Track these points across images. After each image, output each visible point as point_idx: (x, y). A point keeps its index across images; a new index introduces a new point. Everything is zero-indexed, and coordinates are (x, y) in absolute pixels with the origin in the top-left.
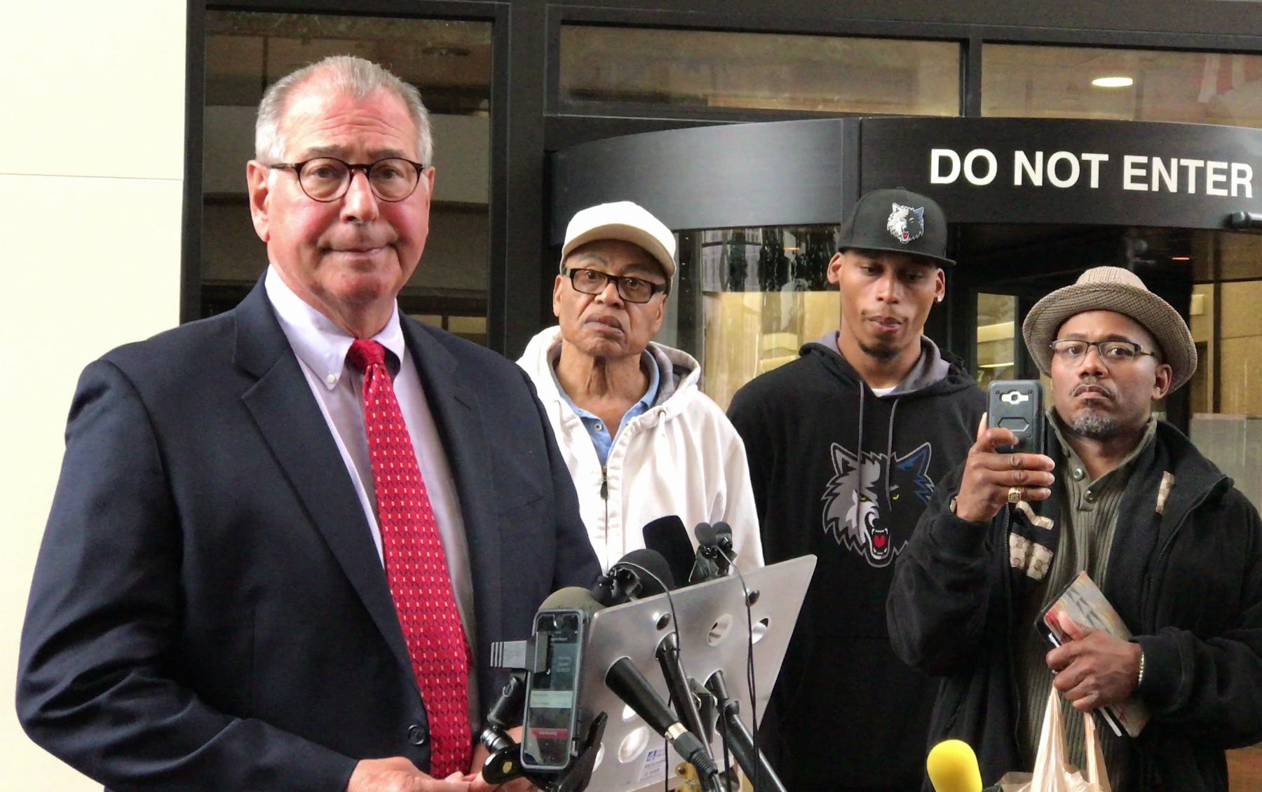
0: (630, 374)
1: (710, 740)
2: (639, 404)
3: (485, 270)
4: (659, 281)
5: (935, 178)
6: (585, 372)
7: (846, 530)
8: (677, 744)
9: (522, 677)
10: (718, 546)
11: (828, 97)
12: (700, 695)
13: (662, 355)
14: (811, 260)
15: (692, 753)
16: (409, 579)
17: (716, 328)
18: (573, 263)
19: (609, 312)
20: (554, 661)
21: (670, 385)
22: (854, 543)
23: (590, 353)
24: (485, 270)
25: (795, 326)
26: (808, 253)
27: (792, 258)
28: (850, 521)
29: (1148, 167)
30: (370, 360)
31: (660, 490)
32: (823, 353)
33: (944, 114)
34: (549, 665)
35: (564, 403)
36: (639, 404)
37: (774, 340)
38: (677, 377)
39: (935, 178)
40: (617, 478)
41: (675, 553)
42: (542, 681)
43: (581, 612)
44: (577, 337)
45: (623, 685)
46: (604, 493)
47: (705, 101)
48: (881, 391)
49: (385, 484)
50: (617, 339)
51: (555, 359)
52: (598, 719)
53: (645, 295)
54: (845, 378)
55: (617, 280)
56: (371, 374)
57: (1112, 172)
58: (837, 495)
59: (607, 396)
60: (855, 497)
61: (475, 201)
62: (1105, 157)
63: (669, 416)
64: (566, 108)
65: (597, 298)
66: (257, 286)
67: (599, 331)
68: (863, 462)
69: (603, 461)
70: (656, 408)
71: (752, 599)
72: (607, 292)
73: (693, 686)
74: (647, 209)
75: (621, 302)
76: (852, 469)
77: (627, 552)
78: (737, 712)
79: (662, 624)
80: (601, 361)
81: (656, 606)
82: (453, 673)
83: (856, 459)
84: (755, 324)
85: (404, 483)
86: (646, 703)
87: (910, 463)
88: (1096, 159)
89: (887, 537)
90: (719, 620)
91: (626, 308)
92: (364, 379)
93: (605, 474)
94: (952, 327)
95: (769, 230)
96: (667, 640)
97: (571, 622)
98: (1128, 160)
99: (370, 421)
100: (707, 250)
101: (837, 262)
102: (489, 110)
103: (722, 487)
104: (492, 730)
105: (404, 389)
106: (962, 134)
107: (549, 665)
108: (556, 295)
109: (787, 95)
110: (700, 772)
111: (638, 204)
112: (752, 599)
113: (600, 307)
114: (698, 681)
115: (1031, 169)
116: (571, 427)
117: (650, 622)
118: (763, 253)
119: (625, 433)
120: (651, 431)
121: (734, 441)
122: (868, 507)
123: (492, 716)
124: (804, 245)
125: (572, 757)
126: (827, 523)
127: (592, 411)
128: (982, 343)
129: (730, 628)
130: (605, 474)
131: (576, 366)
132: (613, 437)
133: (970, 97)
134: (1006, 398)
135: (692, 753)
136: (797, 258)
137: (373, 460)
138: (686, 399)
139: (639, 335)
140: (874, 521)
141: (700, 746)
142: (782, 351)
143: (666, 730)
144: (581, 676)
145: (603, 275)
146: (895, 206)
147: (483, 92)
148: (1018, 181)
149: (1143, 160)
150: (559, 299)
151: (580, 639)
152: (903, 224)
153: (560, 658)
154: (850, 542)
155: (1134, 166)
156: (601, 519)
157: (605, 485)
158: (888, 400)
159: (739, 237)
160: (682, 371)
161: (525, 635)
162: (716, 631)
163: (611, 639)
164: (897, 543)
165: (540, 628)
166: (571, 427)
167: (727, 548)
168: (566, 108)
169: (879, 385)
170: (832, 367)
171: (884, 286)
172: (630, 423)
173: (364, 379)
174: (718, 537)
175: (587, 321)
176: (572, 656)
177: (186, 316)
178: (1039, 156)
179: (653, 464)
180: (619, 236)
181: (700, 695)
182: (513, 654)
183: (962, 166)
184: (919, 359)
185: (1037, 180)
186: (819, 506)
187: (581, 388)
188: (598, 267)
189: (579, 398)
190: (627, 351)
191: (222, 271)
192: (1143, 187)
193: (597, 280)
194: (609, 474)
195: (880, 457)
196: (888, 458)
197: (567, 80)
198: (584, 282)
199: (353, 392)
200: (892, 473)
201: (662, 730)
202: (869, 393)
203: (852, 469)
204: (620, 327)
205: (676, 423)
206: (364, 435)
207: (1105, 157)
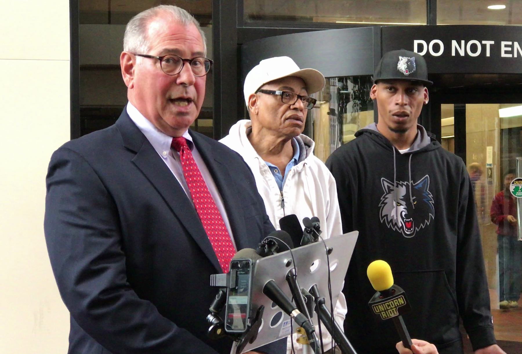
1: (311, 316)
2: (293, 160)
7: (392, 220)
8: (296, 319)
9: (225, 290)
10: (314, 227)
12: (306, 296)
14: (361, 93)
15: (303, 323)
17: (317, 123)
22: (396, 227)
26: (359, 90)
28: (393, 216)
29: (512, 46)
34: (237, 284)
36: (293, 160)
42: (234, 291)
43: (251, 260)
45: (270, 292)
48: (402, 151)
52: (260, 309)
57: (496, 49)
60: (394, 203)
62: (493, 42)
64: (246, 24)
68: (397, 187)
69: (281, 189)
71: (329, 252)
73: (303, 293)
76: (392, 190)
78: (324, 303)
79: (288, 264)
81: (286, 256)
87: (420, 186)
93: (282, 195)
94: (430, 119)
95: (341, 79)
96: (291, 272)
97: (246, 265)
98: (503, 43)
101: (375, 89)
103: (328, 198)
104: (212, 315)
105: (195, 155)
106: (428, 33)
107: (237, 284)
109: (348, 16)
110: (307, 331)
114: (305, 289)
115: (460, 48)
117: (283, 263)
119: (289, 175)
120: (299, 173)
122: (402, 208)
123: (212, 308)
125: (248, 326)
126: (382, 218)
133: (431, 15)
135: (303, 323)
136: (354, 92)
140: (405, 215)
141: (307, 319)
144: (251, 289)
147: (209, 17)
148: (453, 54)
149: (510, 43)
153: (242, 281)
155: (506, 46)
158: (407, 155)
168: (246, 24)
169: (401, 148)
170: (377, 140)
171: (399, 98)
174: (314, 224)
177: (74, 134)
178: (463, 42)
179: (303, 190)
181: (306, 296)
185: (462, 53)
186: (378, 209)
192: (510, 56)
194: (284, 195)
195: (405, 183)
196: (410, 185)
200: (416, 192)
201: (289, 313)
202: (397, 152)
203: (392, 190)
207: (493, 42)
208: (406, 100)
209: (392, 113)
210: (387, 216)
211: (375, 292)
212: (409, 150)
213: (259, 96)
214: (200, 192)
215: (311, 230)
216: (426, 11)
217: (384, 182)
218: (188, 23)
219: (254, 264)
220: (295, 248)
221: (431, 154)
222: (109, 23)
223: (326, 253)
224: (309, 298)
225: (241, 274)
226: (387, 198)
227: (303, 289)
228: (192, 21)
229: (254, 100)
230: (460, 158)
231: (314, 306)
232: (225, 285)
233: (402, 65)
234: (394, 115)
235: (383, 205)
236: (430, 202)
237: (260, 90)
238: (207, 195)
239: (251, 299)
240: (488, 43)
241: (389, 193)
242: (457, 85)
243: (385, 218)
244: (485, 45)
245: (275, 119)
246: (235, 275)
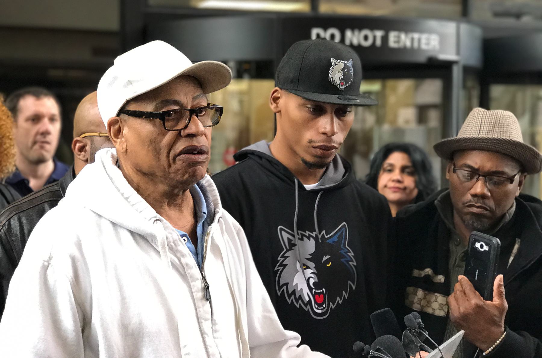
7: (294, 292)
22: (300, 302)
48: (309, 187)
57: (385, 39)
68: (302, 239)
74: (188, 57)
87: (336, 239)
88: (379, 34)
122: (309, 272)
126: (280, 288)
134: (478, 245)
146: (333, 61)
152: (341, 75)
154: (297, 301)
158: (314, 192)
164: (332, 299)
202: (301, 187)
210: (287, 284)
212: (317, 186)
213: (125, 121)
217: (283, 232)
221: (346, 190)
229: (117, 127)
230: (374, 190)
236: (351, 263)
237: (123, 111)
241: (290, 249)
243: (285, 287)
245: (159, 159)
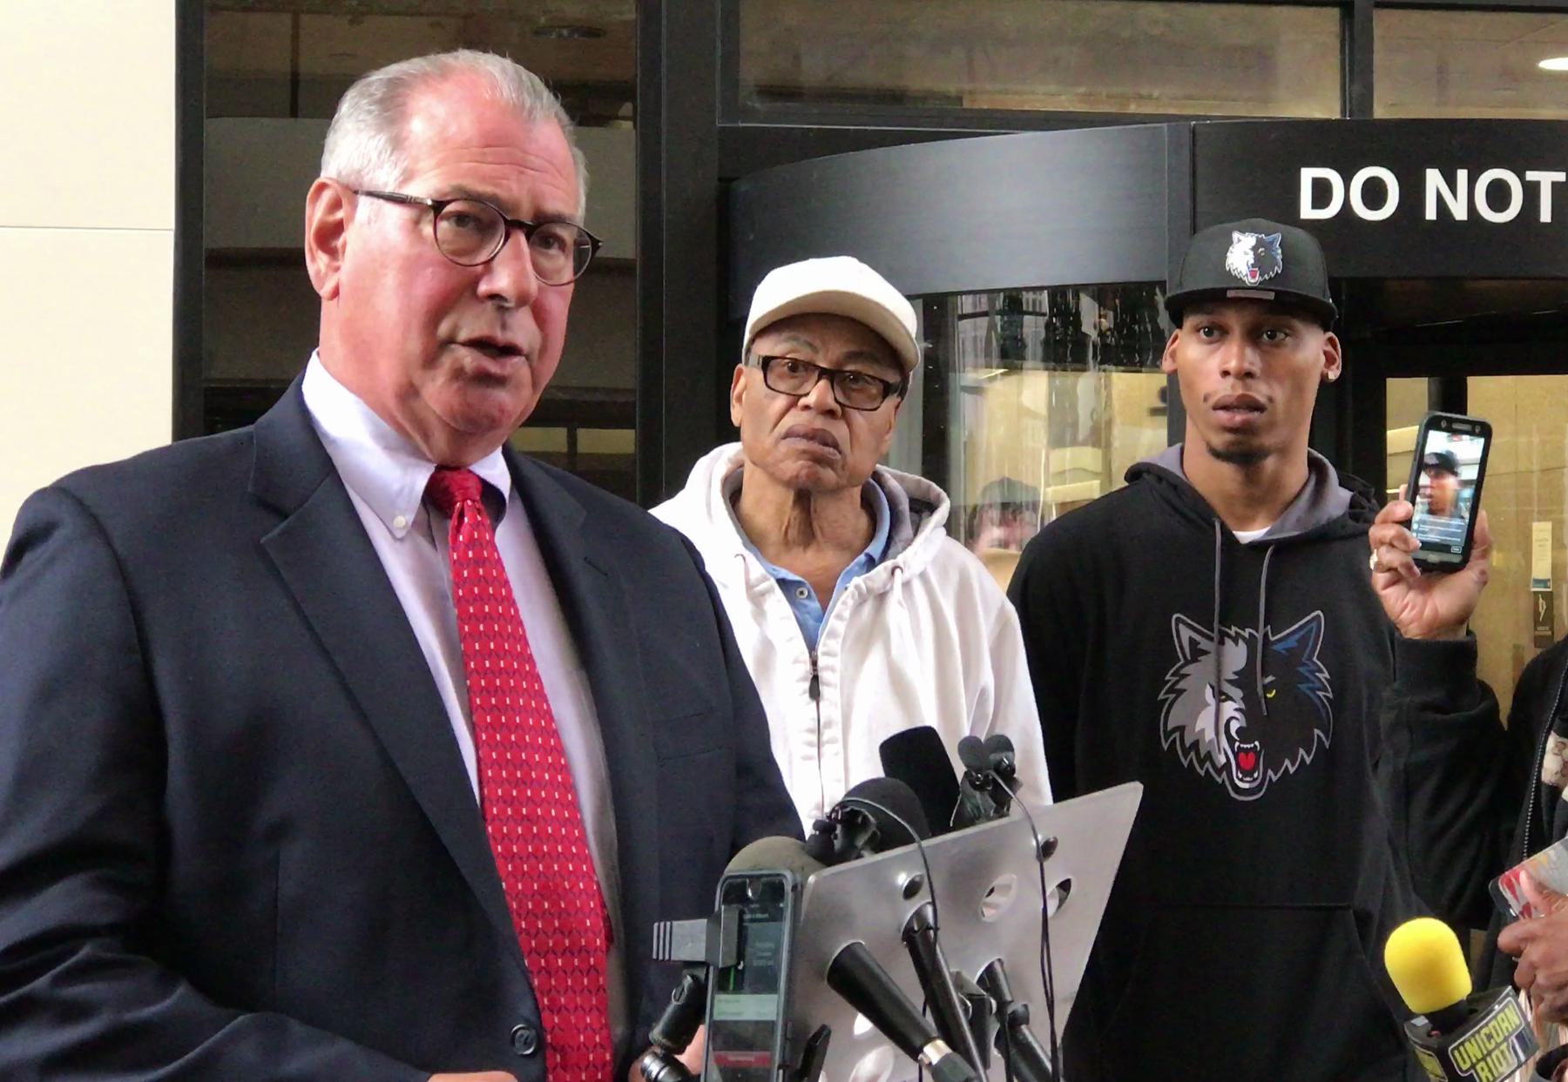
0: (846, 514)
1: (986, 1064)
2: (862, 558)
3: (642, 355)
4: (893, 378)
5: (1307, 212)
6: (780, 511)
11: (1144, 92)
12: (971, 997)
13: (893, 483)
16: (517, 811)
18: (766, 347)
19: (819, 423)
20: (749, 950)
21: (906, 530)
22: (1208, 764)
23: (788, 484)
24: (642, 355)
25: (1100, 437)
26: (1118, 326)
27: (1093, 335)
28: (1203, 731)
30: (458, 495)
31: (899, 686)
32: (1160, 479)
33: (1318, 113)
35: (751, 557)
36: (862, 558)
37: (1068, 457)
38: (916, 517)
39: (1307, 212)
40: (833, 669)
41: (925, 782)
42: (732, 979)
43: (788, 874)
44: (770, 459)
45: (855, 983)
46: (815, 692)
47: (960, 99)
48: (1246, 536)
49: (481, 672)
50: (829, 463)
51: (734, 493)
53: (872, 398)
54: (1193, 516)
55: (833, 375)
56: (461, 515)
58: (1182, 691)
59: (813, 548)
61: (621, 256)
62: (1560, 177)
63: (907, 575)
64: (748, 114)
65: (803, 401)
66: (290, 390)
67: (804, 452)
68: (1222, 643)
69: (812, 646)
70: (889, 564)
71: (1047, 850)
72: (817, 392)
73: (960, 983)
75: (837, 408)
76: (1205, 653)
77: (855, 782)
78: (1026, 1021)
79: (911, 890)
80: (804, 496)
81: (903, 863)
82: (584, 952)
83: (1211, 639)
84: (1037, 435)
85: (508, 672)
86: (888, 1008)
87: (1292, 642)
89: (1258, 754)
90: (998, 882)
91: (845, 417)
92: (451, 524)
93: (814, 663)
96: (919, 915)
97: (773, 890)
99: (458, 581)
100: (965, 325)
102: (633, 119)
103: (987, 678)
104: (656, 1055)
105: (510, 543)
106: (1346, 143)
107: (741, 956)
108: (734, 394)
111: (861, 260)
112: (1047, 850)
113: (805, 415)
114: (965, 974)
115: (1451, 195)
116: (763, 594)
117: (894, 887)
118: (1049, 326)
119: (843, 601)
120: (882, 597)
121: (1002, 609)
122: (1229, 709)
123: (656, 1033)
124: (1111, 314)
126: (1168, 734)
127: (796, 573)
128: (1396, 454)
129: (1012, 900)
130: (814, 663)
131: (768, 503)
132: (824, 608)
133: (1357, 88)
136: (1101, 334)
137: (464, 638)
138: (929, 546)
139: (861, 460)
141: (972, 1074)
142: (1080, 473)
143: (920, 1050)
145: (810, 366)
147: (623, 92)
148: (1431, 213)
150: (739, 399)
151: (788, 914)
153: (758, 945)
154: (1202, 762)
156: (810, 731)
157: (815, 679)
158: (1258, 547)
159: (1013, 302)
160: (923, 507)
161: (703, 909)
162: (993, 898)
163: (833, 914)
165: (727, 900)
166: (763, 594)
167: (1008, 773)
168: (748, 114)
169: (1245, 523)
171: (1232, 354)
172: (851, 586)
173: (451, 524)
174: (994, 757)
175: (787, 435)
176: (776, 942)
178: (1462, 175)
180: (833, 309)
181: (971, 997)
182: (687, 939)
183: (1346, 193)
184: (1305, 484)
185: (1460, 212)
187: (774, 536)
188: (803, 354)
189: (772, 550)
190: (844, 482)
191: (232, 366)
193: (801, 373)
196: (1260, 636)
197: (752, 72)
198: (781, 377)
199: (433, 541)
200: (1264, 658)
201: (914, 1052)
203: (1205, 653)
204: (836, 446)
205: (917, 586)
206: (451, 602)
207: (1560, 177)
208: (1252, 359)
209: (1212, 401)
210: (1181, 729)
211: (1411, 1015)
214: (496, 655)
215: (986, 776)
216: (1338, 77)
218: (539, 114)
219: (798, 889)
220: (934, 835)
222: (294, 113)
223: (1034, 853)
224: (979, 1004)
225: (753, 921)
226: (1185, 676)
227: (958, 974)
228: (553, 111)
231: (994, 1028)
232: (701, 957)
233: (1241, 255)
234: (1216, 408)
235: (1172, 696)
238: (521, 665)
239: (789, 1003)
240: (1546, 179)
241: (1194, 660)
242: (1429, 318)
243: (1177, 735)
244: (1537, 185)
246: (735, 927)
